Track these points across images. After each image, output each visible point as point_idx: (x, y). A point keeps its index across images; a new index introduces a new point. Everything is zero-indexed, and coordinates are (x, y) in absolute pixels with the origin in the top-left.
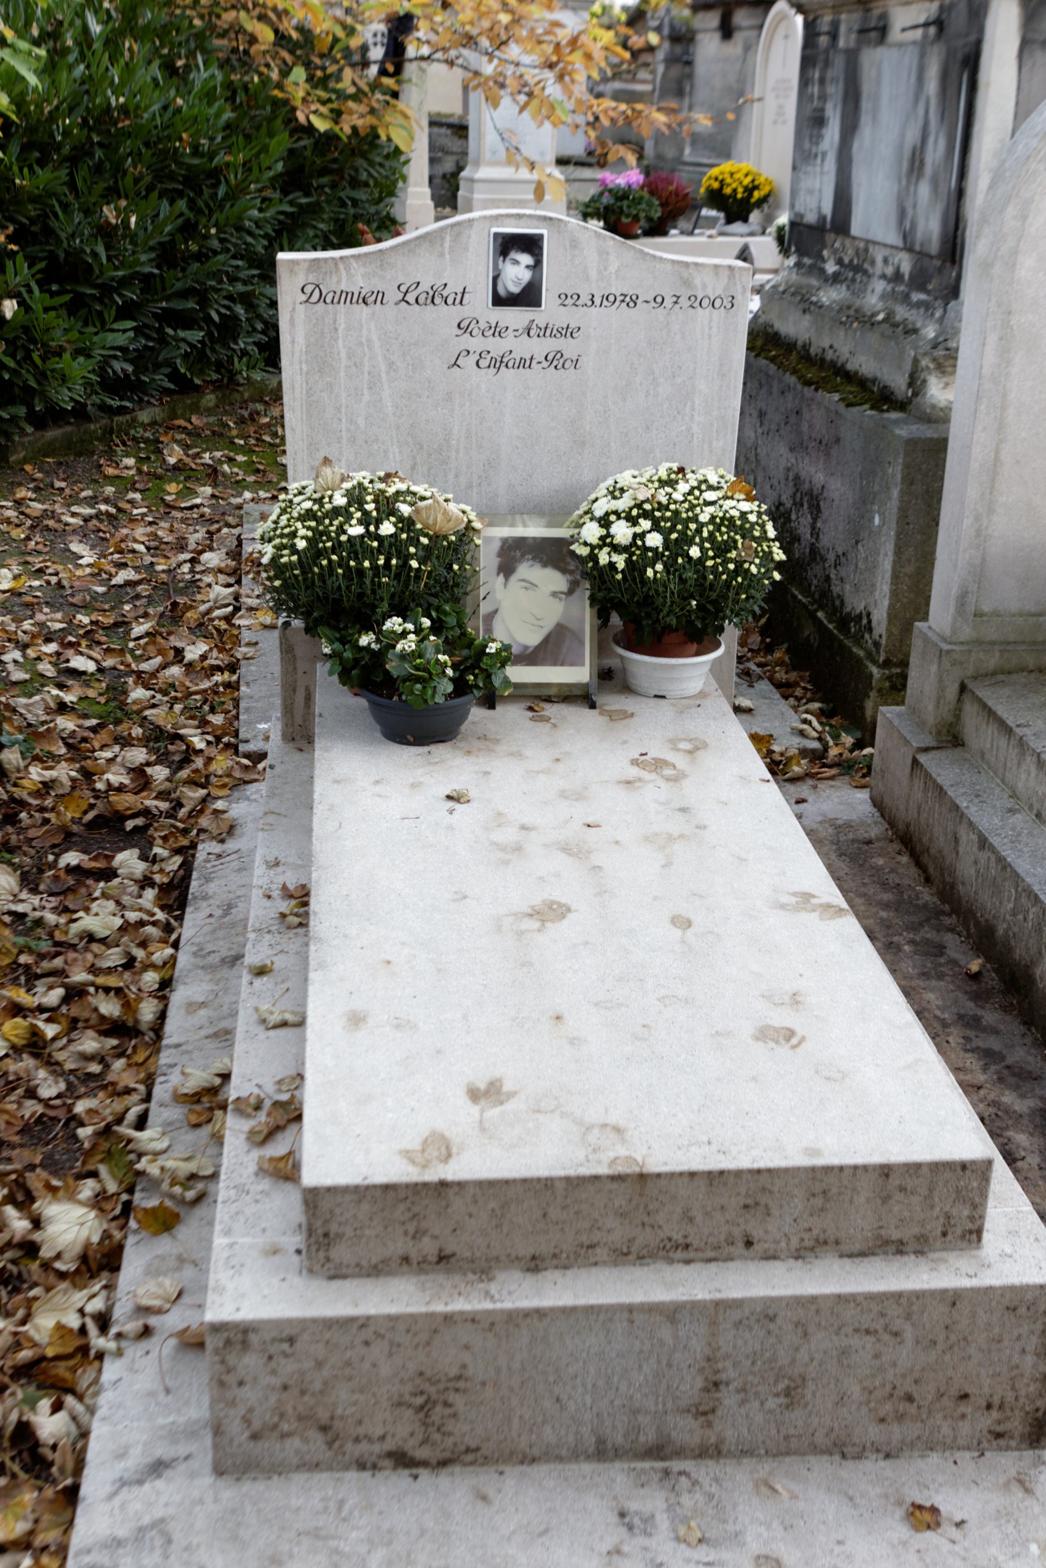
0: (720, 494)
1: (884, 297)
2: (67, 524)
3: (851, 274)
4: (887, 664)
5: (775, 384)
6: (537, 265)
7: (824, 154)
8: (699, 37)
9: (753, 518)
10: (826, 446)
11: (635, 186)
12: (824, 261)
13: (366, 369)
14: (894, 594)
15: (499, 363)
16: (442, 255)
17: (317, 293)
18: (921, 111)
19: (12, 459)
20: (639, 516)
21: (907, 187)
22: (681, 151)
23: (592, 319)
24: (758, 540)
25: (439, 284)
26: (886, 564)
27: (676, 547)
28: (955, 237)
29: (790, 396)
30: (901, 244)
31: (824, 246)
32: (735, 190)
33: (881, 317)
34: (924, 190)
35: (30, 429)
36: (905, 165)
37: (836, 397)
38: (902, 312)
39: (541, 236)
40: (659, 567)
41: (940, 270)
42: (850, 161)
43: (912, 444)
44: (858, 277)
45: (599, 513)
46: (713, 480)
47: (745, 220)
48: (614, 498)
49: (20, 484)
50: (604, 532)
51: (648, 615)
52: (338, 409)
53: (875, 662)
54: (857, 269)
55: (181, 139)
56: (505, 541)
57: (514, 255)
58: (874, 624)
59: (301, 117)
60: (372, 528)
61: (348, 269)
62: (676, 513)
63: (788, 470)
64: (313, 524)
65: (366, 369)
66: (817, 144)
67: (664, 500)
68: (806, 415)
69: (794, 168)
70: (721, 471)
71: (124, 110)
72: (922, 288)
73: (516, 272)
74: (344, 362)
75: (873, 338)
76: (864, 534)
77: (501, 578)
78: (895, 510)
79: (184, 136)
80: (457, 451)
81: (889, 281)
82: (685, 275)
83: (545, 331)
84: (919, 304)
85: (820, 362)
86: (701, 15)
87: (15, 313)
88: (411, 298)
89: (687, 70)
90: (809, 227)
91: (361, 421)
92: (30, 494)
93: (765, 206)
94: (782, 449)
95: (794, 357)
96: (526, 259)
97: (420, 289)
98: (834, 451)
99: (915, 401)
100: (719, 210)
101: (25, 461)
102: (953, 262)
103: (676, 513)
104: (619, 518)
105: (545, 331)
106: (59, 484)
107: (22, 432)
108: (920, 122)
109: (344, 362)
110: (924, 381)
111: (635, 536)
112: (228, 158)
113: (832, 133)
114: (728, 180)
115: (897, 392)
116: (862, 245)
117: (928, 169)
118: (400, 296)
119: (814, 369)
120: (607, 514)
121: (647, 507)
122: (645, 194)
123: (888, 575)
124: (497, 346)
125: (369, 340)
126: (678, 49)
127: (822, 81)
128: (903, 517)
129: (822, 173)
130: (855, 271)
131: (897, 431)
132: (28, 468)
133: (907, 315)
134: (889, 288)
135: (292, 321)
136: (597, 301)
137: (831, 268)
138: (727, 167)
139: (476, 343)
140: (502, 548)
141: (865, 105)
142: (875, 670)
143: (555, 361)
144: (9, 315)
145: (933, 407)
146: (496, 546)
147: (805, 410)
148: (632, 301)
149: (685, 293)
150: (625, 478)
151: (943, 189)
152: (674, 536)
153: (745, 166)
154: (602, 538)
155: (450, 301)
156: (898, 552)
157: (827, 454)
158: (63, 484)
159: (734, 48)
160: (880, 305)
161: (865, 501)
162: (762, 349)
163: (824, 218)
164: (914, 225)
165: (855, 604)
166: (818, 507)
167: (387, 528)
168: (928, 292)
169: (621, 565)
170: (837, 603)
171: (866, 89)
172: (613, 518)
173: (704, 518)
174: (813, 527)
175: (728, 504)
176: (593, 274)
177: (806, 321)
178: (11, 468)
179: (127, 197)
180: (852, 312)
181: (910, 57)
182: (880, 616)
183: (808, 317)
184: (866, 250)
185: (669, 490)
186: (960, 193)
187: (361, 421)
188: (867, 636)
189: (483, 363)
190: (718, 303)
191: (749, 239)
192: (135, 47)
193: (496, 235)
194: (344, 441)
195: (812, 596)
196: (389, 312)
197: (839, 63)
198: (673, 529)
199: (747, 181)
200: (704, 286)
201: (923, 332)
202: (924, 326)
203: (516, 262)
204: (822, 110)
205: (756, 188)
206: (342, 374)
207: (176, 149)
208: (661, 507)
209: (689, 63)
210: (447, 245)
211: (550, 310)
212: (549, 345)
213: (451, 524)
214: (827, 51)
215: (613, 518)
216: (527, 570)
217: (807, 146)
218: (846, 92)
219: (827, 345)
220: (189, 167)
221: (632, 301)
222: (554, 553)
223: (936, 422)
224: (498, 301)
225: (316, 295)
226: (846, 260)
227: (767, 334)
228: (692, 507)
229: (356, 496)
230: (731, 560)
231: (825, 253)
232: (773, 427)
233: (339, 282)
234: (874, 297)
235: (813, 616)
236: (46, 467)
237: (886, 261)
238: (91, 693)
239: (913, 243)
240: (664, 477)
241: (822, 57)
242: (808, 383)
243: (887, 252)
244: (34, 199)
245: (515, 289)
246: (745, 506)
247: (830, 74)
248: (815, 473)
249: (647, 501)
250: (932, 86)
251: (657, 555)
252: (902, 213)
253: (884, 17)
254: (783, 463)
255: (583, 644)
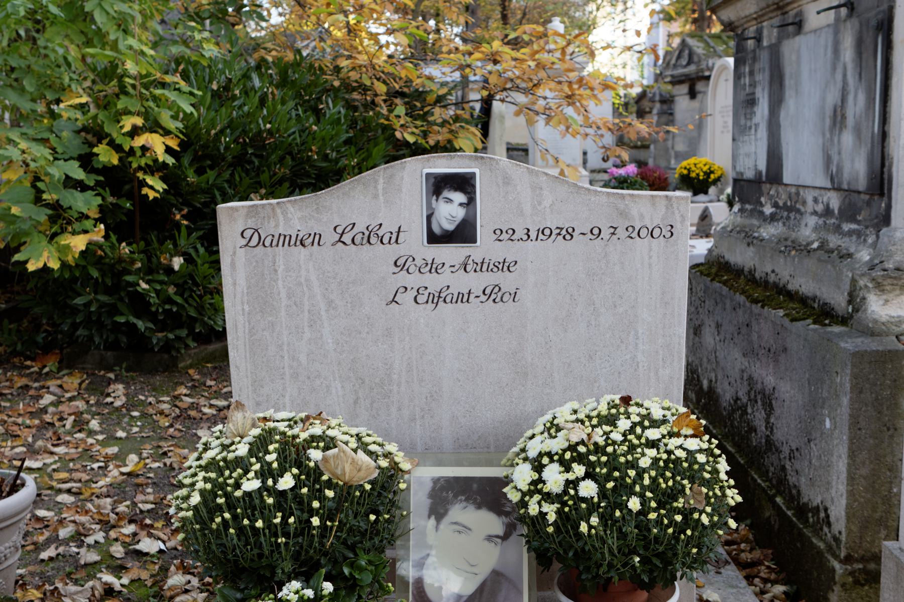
0: (664, 430)
1: (816, 229)
2: (204, 414)
3: (786, 214)
4: (848, 560)
5: (728, 302)
6: (471, 202)
7: (757, 125)
8: (677, 99)
9: (702, 458)
10: (776, 354)
11: (631, 175)
12: (762, 205)
13: (306, 308)
14: (851, 494)
15: (437, 299)
16: (376, 196)
17: (256, 238)
18: (839, 76)
19: (181, 365)
20: (573, 460)
21: (832, 139)
22: (669, 162)
23: (528, 253)
24: (708, 484)
25: (374, 224)
26: (841, 465)
27: (613, 498)
28: (882, 173)
29: (740, 312)
30: (829, 186)
31: (761, 194)
32: (698, 175)
33: (815, 245)
34: (847, 138)
35: (192, 344)
36: (828, 122)
37: (781, 313)
38: (834, 241)
39: (473, 175)
40: (594, 520)
41: (868, 203)
42: (779, 126)
43: (859, 356)
44: (792, 215)
45: (532, 454)
46: (657, 414)
47: (706, 193)
48: (552, 437)
49: (182, 384)
50: (536, 476)
51: (588, 569)
52: (280, 347)
53: (836, 557)
54: (790, 209)
55: (311, 150)
56: (436, 481)
57: (447, 194)
58: (832, 519)
59: (398, 135)
60: (270, 482)
61: (285, 213)
62: (614, 456)
63: (743, 371)
64: (213, 475)
65: (306, 308)
66: (751, 119)
67: (601, 441)
68: (755, 327)
69: (734, 140)
70: (667, 403)
71: (270, 132)
72: (852, 219)
73: (450, 211)
74: (285, 302)
75: (810, 263)
76: (816, 434)
77: (432, 522)
78: (846, 417)
79: (313, 148)
80: (399, 385)
81: (820, 216)
82: (622, 206)
83: (481, 266)
84: (850, 233)
85: (765, 284)
86: (677, 87)
87: (181, 265)
88: (347, 238)
89: (671, 118)
90: (749, 181)
91: (303, 358)
92: (185, 391)
93: (719, 183)
94: (737, 354)
95: (742, 280)
96: (459, 197)
97: (355, 230)
98: (782, 358)
99: (856, 316)
100: (688, 189)
101: (191, 366)
102: (882, 194)
103: (614, 456)
104: (552, 461)
105: (481, 266)
106: (209, 383)
107: (187, 347)
108: (839, 85)
109: (285, 302)
110: (864, 298)
111: (568, 482)
112: (347, 162)
113: (762, 109)
114: (693, 168)
115: (837, 308)
116: (793, 190)
117: (850, 121)
118: (337, 237)
119: (759, 290)
120: (541, 455)
121: (582, 449)
122: (639, 180)
123: (844, 476)
124: (434, 282)
125: (307, 280)
126: (665, 107)
127: (752, 73)
128: (854, 423)
129: (756, 140)
130: (790, 210)
131: (843, 345)
132: (191, 371)
133: (839, 243)
134: (821, 222)
135: (233, 264)
136: (533, 235)
137: (768, 210)
138: (692, 161)
139: (413, 280)
140: (433, 489)
141: (788, 82)
142: (837, 565)
143: (492, 294)
144: (176, 267)
145: (875, 321)
146: (429, 486)
147: (754, 323)
148: (569, 234)
149: (622, 224)
150: (564, 414)
151: (866, 135)
152: (610, 485)
153: (704, 160)
154: (534, 483)
155: (385, 240)
156: (852, 455)
157: (776, 361)
158: (213, 383)
159: (695, 104)
160: (814, 236)
161: (815, 405)
162: (716, 275)
163: (760, 173)
164: (840, 169)
165: (812, 496)
166: (771, 405)
167: (286, 482)
168: (858, 222)
169: (552, 518)
170: (794, 492)
171: (788, 70)
172: (545, 460)
173: (645, 463)
174: (767, 422)
175: (673, 443)
176: (527, 209)
177: (750, 252)
178: (179, 372)
179: (266, 188)
180: (789, 243)
181: (826, 38)
182: (838, 511)
183: (752, 248)
184: (798, 194)
185: (607, 428)
186: (884, 135)
187: (303, 358)
188: (826, 529)
189: (421, 299)
190: (656, 233)
191: (709, 205)
192: (276, 92)
193: (427, 175)
194: (287, 377)
195: (770, 481)
196: (327, 252)
197: (764, 57)
198: (608, 477)
199: (705, 169)
200: (642, 216)
201: (858, 256)
202: (858, 251)
203: (450, 201)
204: (754, 93)
205: (712, 172)
206: (283, 313)
207: (308, 156)
208: (598, 449)
209: (671, 114)
210: (380, 187)
211: (485, 246)
212: (487, 279)
213: (362, 474)
214: (754, 51)
215: (545, 460)
216: (462, 513)
217: (743, 122)
218: (772, 77)
219: (769, 271)
220: (321, 169)
221: (569, 234)
222: (489, 494)
223: (879, 335)
224: (434, 238)
225: (255, 239)
226: (781, 203)
227: (720, 263)
228: (632, 448)
229: (259, 446)
230: (679, 511)
231: (763, 199)
232: (728, 336)
233: (277, 226)
234: (808, 230)
235: (771, 499)
236: (205, 370)
237: (816, 200)
238: (145, 575)
239: (840, 183)
240: (604, 412)
241: (750, 56)
242: (755, 301)
243: (816, 193)
244: (204, 191)
245: (450, 227)
246: (693, 444)
247: (757, 67)
248: (767, 377)
249: (582, 442)
250: (848, 54)
251: (593, 507)
252: (828, 160)
253: (800, 14)
254: (738, 366)
255: (520, 593)
